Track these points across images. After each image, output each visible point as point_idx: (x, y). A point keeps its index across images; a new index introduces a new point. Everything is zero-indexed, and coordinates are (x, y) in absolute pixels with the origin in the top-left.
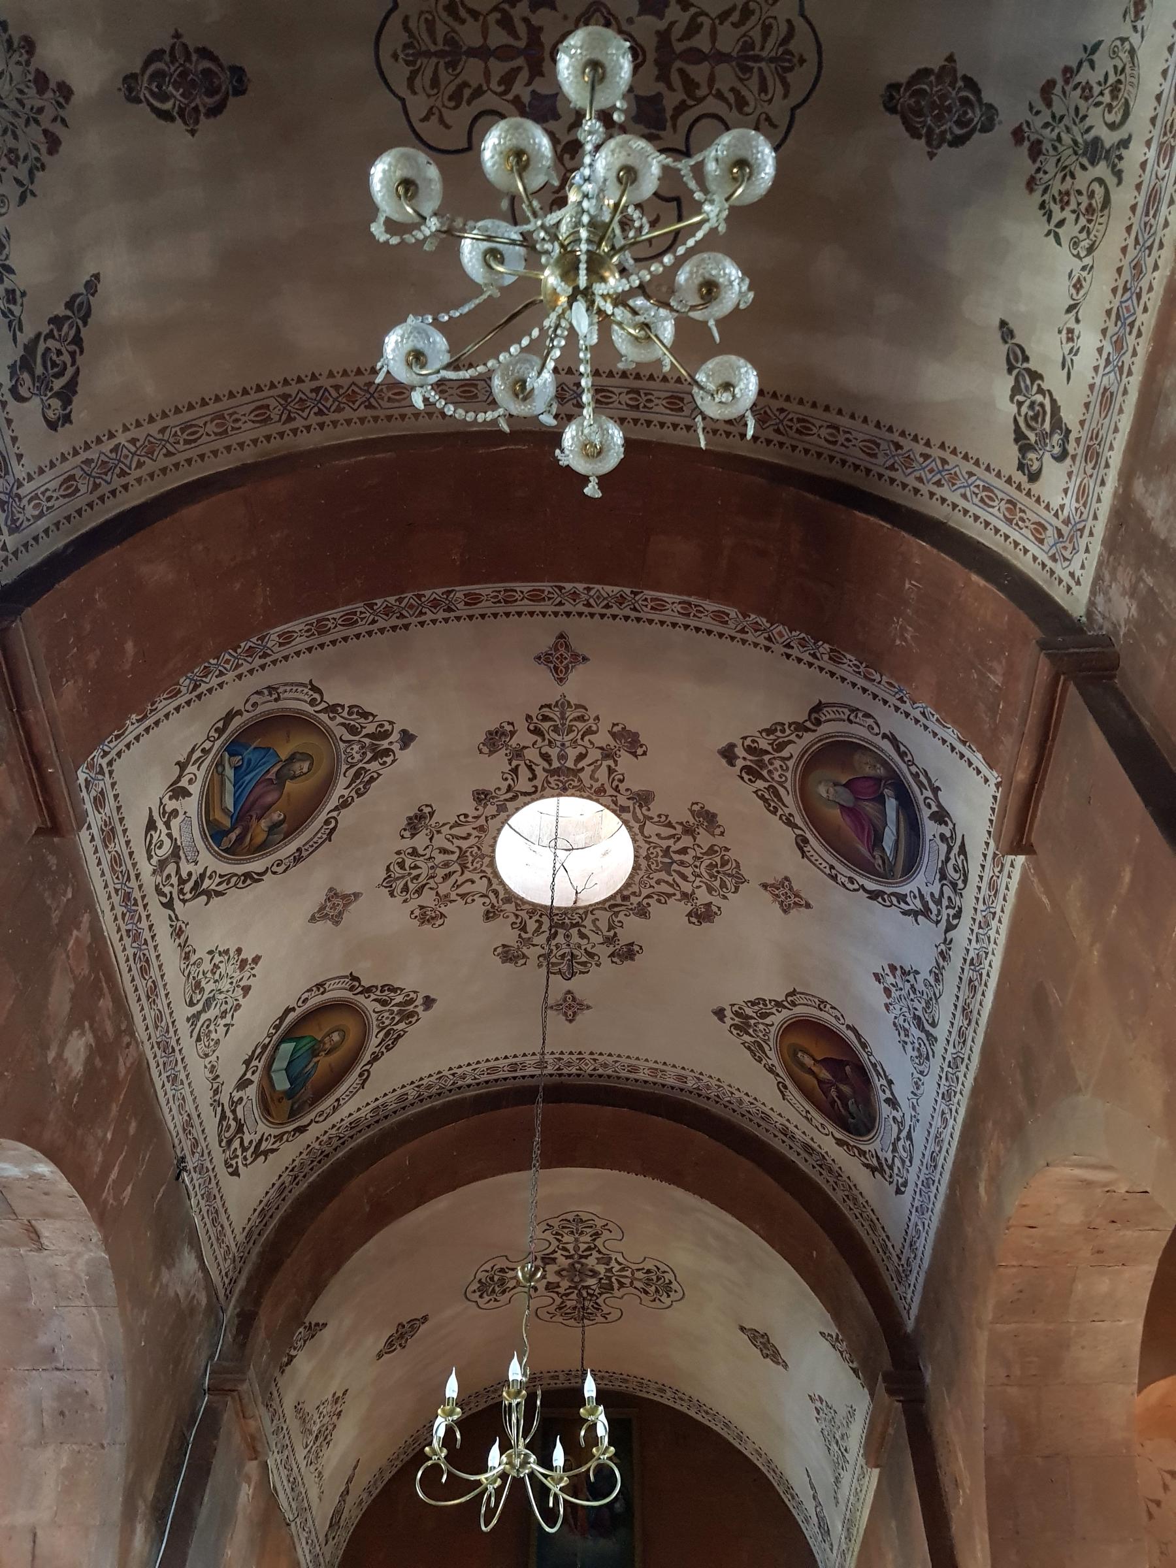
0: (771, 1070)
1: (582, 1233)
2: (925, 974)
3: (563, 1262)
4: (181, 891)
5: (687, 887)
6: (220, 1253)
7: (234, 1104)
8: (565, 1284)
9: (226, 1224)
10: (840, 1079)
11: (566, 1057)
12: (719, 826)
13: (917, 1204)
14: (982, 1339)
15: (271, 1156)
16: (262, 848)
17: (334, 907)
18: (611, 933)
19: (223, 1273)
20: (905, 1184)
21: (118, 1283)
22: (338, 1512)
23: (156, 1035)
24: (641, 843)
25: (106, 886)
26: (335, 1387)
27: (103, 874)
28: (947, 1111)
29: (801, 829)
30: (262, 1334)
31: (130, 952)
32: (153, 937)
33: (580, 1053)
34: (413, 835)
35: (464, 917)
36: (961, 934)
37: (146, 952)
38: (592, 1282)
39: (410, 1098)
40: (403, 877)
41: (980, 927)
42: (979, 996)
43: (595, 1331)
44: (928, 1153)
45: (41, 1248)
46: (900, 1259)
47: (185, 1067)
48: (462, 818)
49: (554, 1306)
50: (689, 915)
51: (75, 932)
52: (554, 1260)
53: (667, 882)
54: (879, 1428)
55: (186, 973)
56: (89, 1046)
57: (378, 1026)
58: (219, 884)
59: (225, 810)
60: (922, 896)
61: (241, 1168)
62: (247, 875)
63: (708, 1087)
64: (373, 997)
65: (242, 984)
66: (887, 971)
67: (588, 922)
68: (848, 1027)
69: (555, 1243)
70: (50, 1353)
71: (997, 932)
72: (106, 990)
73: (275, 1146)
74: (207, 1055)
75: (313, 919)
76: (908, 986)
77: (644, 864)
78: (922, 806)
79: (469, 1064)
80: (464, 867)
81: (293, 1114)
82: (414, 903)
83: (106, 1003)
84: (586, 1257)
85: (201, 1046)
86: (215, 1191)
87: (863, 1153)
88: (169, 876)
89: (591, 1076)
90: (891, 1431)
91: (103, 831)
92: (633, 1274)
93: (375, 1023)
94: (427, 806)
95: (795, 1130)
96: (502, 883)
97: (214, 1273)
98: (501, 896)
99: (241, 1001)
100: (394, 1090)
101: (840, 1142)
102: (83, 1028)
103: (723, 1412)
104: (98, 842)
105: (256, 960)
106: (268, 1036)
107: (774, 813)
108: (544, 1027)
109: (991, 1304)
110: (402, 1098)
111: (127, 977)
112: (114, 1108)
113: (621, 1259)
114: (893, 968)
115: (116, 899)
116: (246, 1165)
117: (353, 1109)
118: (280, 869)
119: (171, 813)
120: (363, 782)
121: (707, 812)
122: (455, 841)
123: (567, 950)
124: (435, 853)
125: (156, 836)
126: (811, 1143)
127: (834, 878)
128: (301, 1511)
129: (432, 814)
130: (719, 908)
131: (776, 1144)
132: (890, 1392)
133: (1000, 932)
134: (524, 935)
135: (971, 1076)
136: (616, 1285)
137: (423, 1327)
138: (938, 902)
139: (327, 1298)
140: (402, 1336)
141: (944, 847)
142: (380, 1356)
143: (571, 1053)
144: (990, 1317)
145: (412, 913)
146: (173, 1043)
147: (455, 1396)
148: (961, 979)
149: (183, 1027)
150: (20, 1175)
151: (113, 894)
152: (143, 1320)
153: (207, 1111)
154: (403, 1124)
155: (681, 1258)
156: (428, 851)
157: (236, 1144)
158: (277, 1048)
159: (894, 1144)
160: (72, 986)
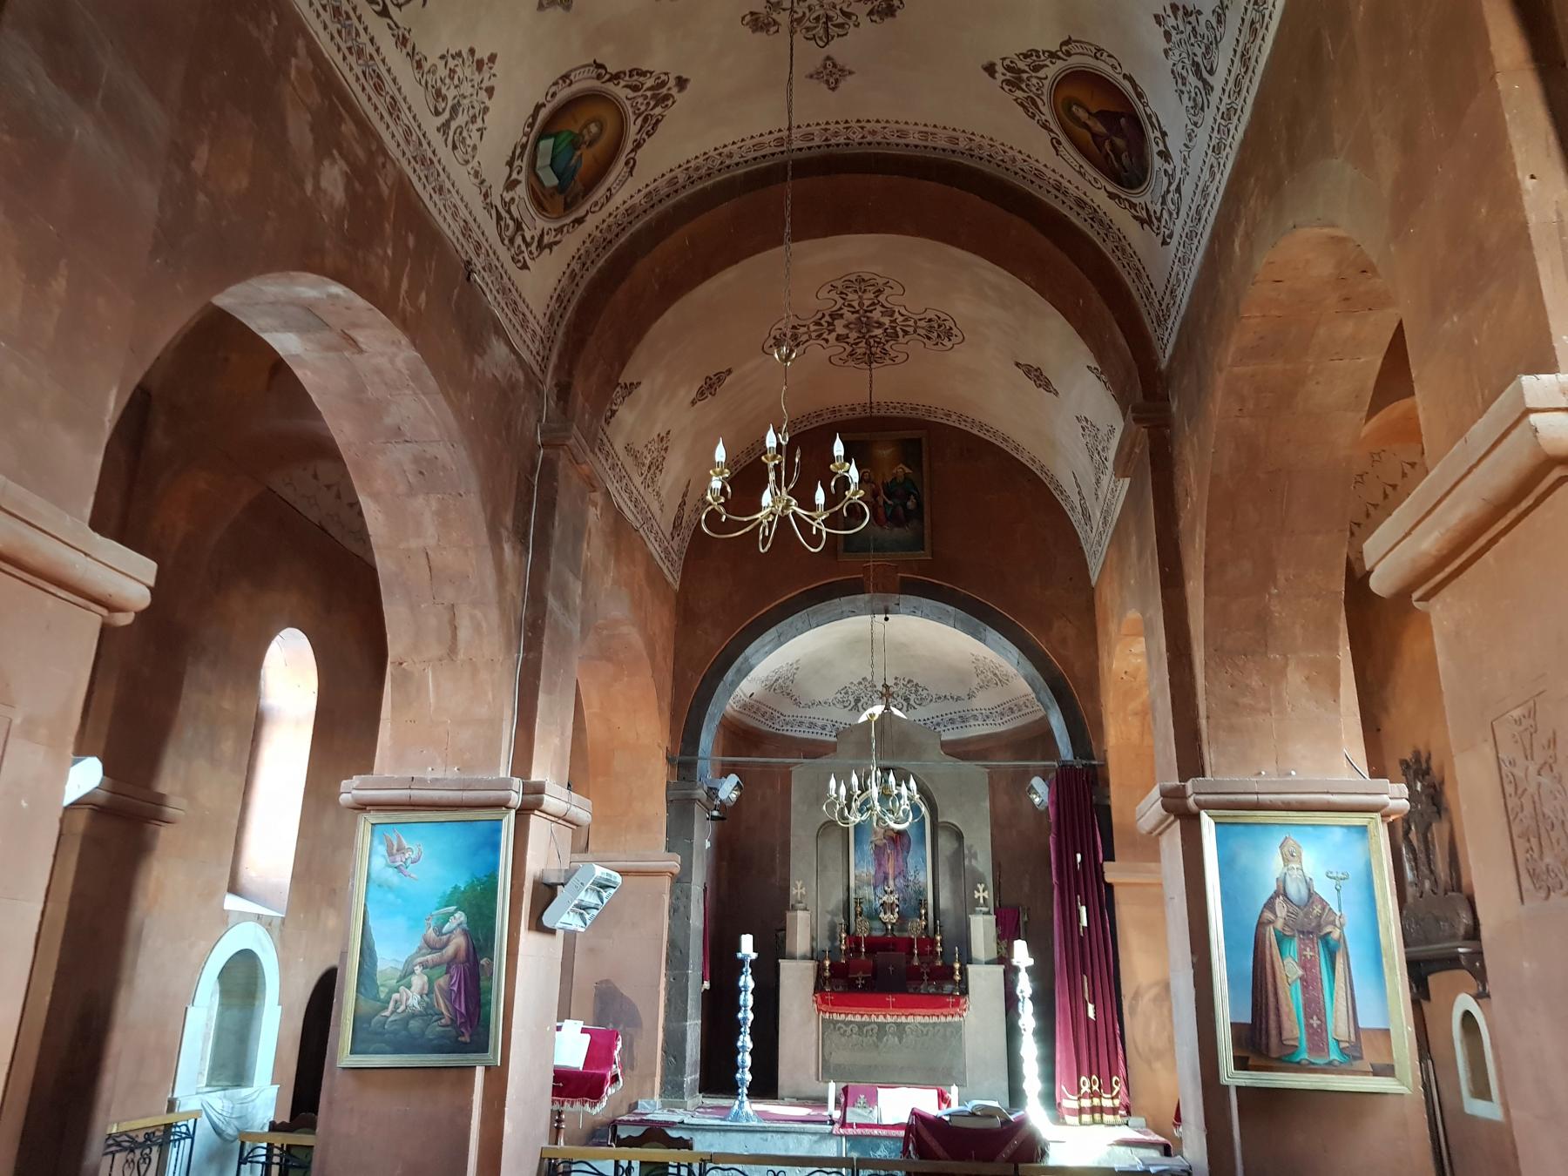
0: (1045, 126)
2: (1207, 15)
8: (853, 335)
10: (1112, 129)
11: (832, 127)
14: (1221, 379)
15: (555, 248)
20: (1171, 236)
26: (659, 429)
30: (580, 399)
32: (378, 50)
38: (878, 332)
42: (1259, 41)
43: (879, 372)
44: (1194, 207)
45: (361, 351)
51: (293, 61)
54: (1127, 449)
63: (980, 147)
64: (622, 83)
65: (484, 85)
66: (1169, 11)
68: (1125, 76)
70: (398, 431)
74: (467, 162)
76: (1189, 28)
81: (568, 207)
83: (348, 128)
85: (459, 153)
87: (1133, 206)
97: (525, 355)
101: (1111, 196)
102: (332, 155)
105: (492, 58)
109: (1232, 349)
110: (673, 181)
111: (363, 98)
114: (1174, 8)
115: (326, 16)
123: (821, 12)
128: (646, 520)
135: (1241, 129)
136: (901, 334)
142: (693, 403)
149: (436, 139)
151: (321, 11)
154: (678, 207)
155: (961, 308)
157: (519, 240)
160: (309, 117)
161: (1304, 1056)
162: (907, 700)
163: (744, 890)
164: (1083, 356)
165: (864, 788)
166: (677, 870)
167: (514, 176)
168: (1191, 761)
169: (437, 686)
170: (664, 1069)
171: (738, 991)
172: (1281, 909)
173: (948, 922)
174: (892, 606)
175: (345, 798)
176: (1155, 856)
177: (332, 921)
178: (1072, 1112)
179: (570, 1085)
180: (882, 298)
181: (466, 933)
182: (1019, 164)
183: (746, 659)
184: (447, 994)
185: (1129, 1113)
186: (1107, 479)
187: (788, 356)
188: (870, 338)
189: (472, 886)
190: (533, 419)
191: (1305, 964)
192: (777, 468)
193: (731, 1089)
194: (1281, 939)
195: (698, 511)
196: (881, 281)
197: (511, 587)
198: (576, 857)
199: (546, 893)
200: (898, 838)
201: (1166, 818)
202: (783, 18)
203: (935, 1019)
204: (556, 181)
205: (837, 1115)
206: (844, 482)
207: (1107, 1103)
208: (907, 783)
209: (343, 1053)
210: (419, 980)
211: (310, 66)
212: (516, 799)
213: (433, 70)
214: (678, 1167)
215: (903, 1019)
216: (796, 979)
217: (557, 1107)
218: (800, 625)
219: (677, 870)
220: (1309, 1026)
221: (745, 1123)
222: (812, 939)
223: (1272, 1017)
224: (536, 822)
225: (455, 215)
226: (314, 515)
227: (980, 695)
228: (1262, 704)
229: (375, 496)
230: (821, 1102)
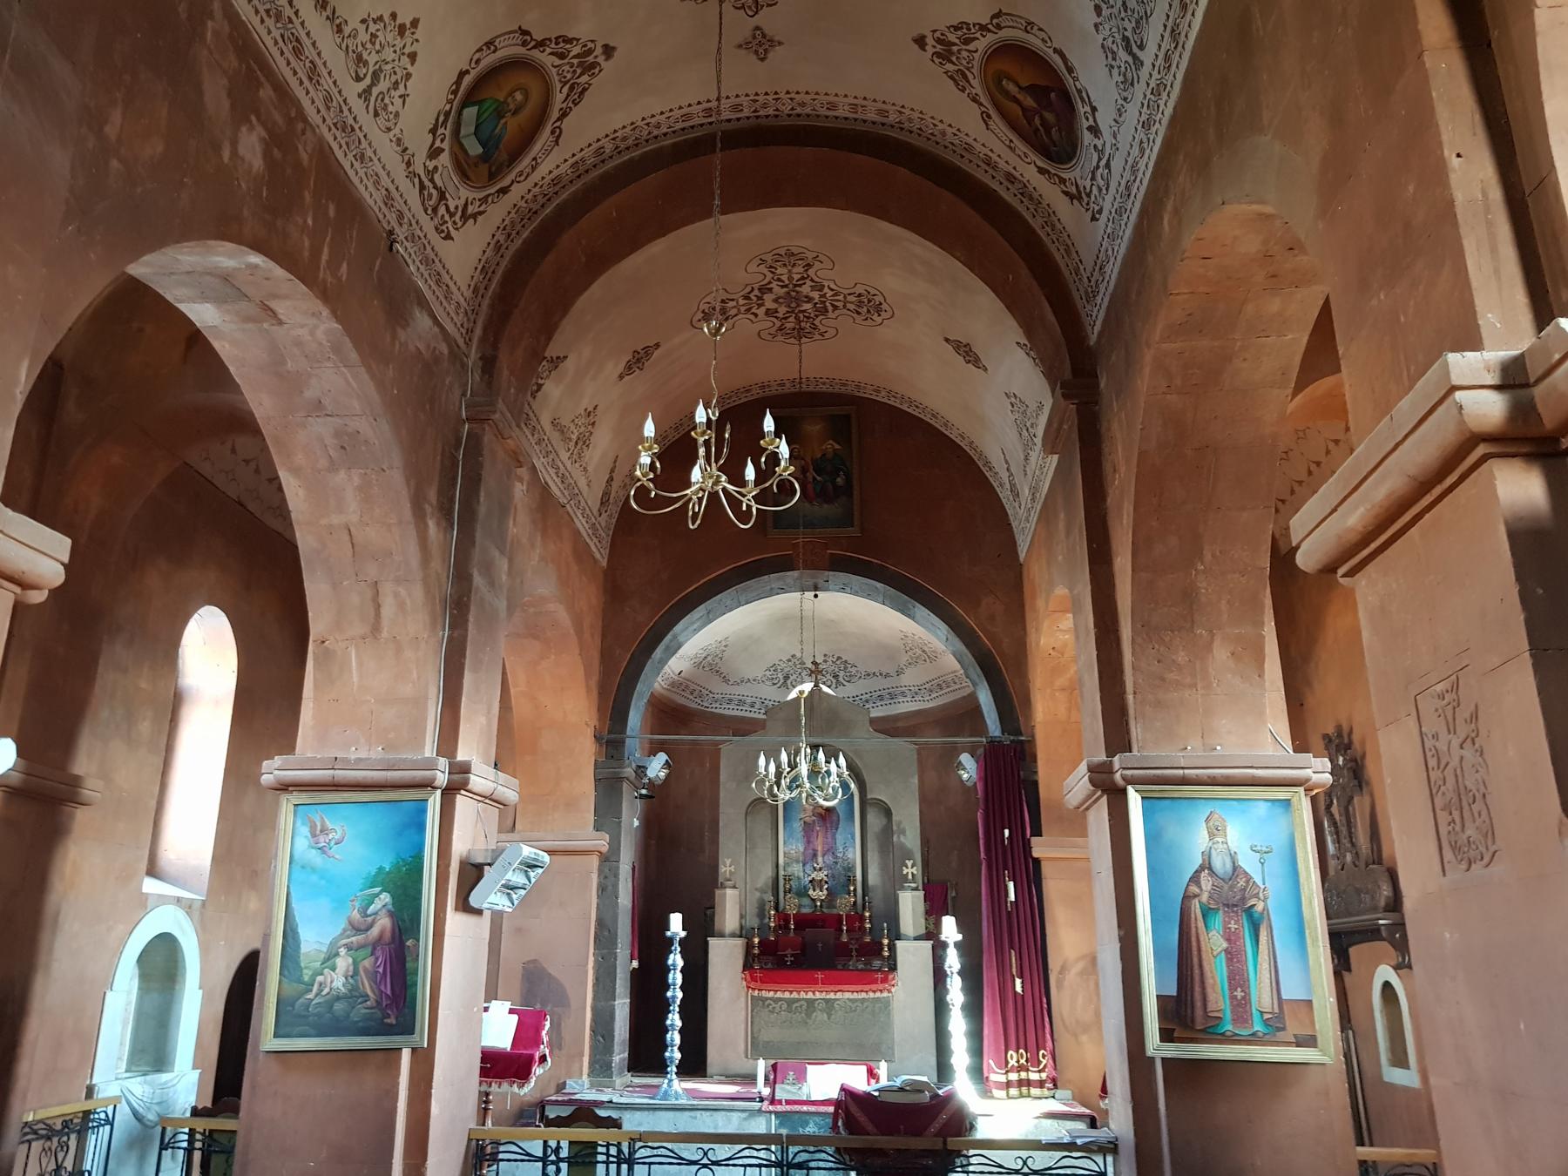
0: (974, 100)
7: (431, 173)
8: (782, 310)
9: (451, 284)
10: (1044, 106)
11: (761, 98)
13: (1109, 230)
14: (1148, 356)
15: (480, 218)
20: (1100, 212)
22: (606, 494)
26: (586, 403)
30: (506, 373)
31: (276, 34)
32: (296, 13)
38: (807, 306)
44: (1123, 183)
45: (281, 323)
51: (210, 24)
56: (262, 140)
64: (548, 50)
65: (407, 51)
68: (1055, 51)
72: (262, 79)
74: (389, 129)
81: (493, 177)
83: (266, 93)
85: (381, 120)
87: (1062, 181)
97: (449, 327)
101: (1041, 171)
105: (415, 23)
108: (719, 82)
109: (1160, 327)
110: (599, 152)
111: (281, 62)
112: (307, 196)
131: (979, 175)
135: (1171, 105)
136: (830, 308)
139: (567, 329)
142: (621, 377)
149: (357, 105)
154: (604, 178)
155: (891, 283)
157: (442, 210)
158: (460, 113)
160: (225, 81)
161: (1228, 1027)
162: (836, 676)
163: (672, 869)
164: (1013, 332)
165: (793, 765)
166: (605, 849)
167: (438, 144)
168: (1117, 737)
169: (360, 664)
171: (666, 970)
172: (1206, 882)
173: (877, 899)
174: (821, 582)
175: (266, 779)
178: (999, 1086)
179: (497, 1066)
180: (811, 272)
181: (391, 914)
182: (949, 137)
183: (675, 637)
184: (373, 976)
185: (1056, 1086)
186: (1036, 454)
189: (397, 867)
190: (457, 392)
191: (1230, 937)
192: (707, 443)
195: (626, 487)
196: (810, 255)
197: (436, 565)
198: (504, 837)
199: (473, 873)
200: (827, 816)
203: (863, 995)
205: (766, 1092)
206: (774, 458)
207: (1034, 1076)
208: (836, 760)
209: (266, 1036)
210: (343, 963)
211: (227, 29)
212: (442, 779)
214: (608, 1146)
215: (832, 996)
216: (725, 957)
217: (484, 1088)
219: (605, 849)
220: (1233, 998)
221: (674, 1101)
222: (742, 916)
223: (1197, 989)
224: (462, 802)
225: (377, 183)
226: (232, 491)
227: (908, 671)
228: (1188, 680)
229: (296, 471)
230: (751, 1079)
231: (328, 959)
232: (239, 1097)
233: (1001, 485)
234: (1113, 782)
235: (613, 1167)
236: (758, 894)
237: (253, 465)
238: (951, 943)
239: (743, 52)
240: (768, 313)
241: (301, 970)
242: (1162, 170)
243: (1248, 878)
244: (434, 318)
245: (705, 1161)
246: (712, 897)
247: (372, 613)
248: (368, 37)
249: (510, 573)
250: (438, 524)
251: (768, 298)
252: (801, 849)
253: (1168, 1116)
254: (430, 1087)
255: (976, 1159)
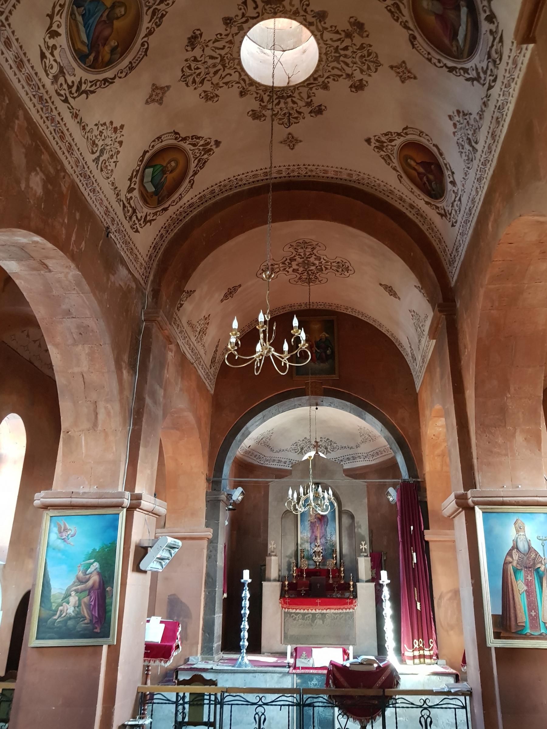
0: (395, 169)
1: (307, 248)
2: (475, 115)
3: (299, 260)
4: (71, 92)
5: (349, 71)
6: (138, 266)
7: (129, 200)
8: (301, 269)
9: (138, 254)
10: (428, 171)
11: (291, 168)
12: (366, 31)
14: (482, 292)
15: (153, 223)
16: (109, 63)
17: (157, 95)
18: (309, 100)
19: (141, 274)
20: (456, 222)
21: (89, 284)
22: (214, 358)
23: (78, 170)
24: (322, 45)
25: (27, 94)
26: (204, 313)
27: (23, 87)
28: (479, 187)
29: (412, 30)
31: (52, 128)
32: (62, 119)
33: (298, 165)
34: (193, 49)
35: (229, 95)
36: (496, 91)
37: (60, 128)
38: (313, 268)
39: (216, 191)
40: (191, 75)
41: (506, 87)
42: (500, 127)
43: (314, 287)
44: (468, 208)
45: (50, 271)
46: (451, 256)
47: (98, 185)
48: (219, 36)
49: (297, 278)
50: (351, 87)
51: (17, 122)
52: (295, 260)
53: (338, 68)
54: (435, 325)
55: (86, 137)
57: (194, 157)
58: (91, 86)
59: (83, 42)
60: (477, 69)
61: (139, 229)
62: (105, 80)
63: (363, 179)
64: (188, 142)
65: (118, 140)
66: (456, 113)
67: (296, 94)
68: (434, 145)
69: (295, 253)
71: (514, 90)
72: (44, 150)
73: (154, 218)
74: (108, 178)
75: (147, 102)
76: (465, 121)
77: (324, 57)
78: (482, 12)
79: (243, 174)
80: (224, 66)
81: (160, 203)
82: (200, 90)
83: (45, 157)
84: (310, 258)
85: (104, 173)
86: (129, 240)
87: (437, 208)
88: (61, 85)
89: (305, 176)
90: (440, 326)
91: (16, 62)
92: (331, 263)
93: (192, 156)
94: (198, 30)
95: (405, 197)
96: (247, 75)
97: (137, 275)
98: (247, 82)
99: (119, 149)
100: (208, 188)
101: (427, 203)
102: (36, 170)
103: (372, 317)
104: (15, 68)
105: (122, 127)
106: (138, 166)
107: (397, 20)
109: (487, 277)
110: (213, 192)
111: (54, 143)
112: (65, 209)
113: (325, 258)
114: (458, 112)
115: (35, 100)
116: (141, 227)
117: (189, 199)
118: (123, 75)
119: (52, 47)
120: (158, 17)
121: (359, 22)
122: (217, 50)
123: (286, 111)
124: (207, 59)
125: (47, 62)
126: (413, 204)
127: (430, 60)
129: (201, 35)
130: (367, 82)
132: (440, 311)
133: (515, 89)
134: (263, 104)
136: (324, 269)
137: (239, 289)
138: (485, 73)
139: (196, 275)
140: (231, 293)
141: (491, 38)
142: (222, 301)
143: (294, 165)
144: (486, 282)
145: (200, 95)
146: (89, 173)
147: (237, 328)
148: (492, 117)
150: (28, 242)
152: (106, 296)
153: (115, 205)
155: (353, 256)
156: (203, 58)
159: (453, 204)
160: (24, 150)
161: (528, 631)
162: (326, 448)
163: (244, 547)
164: (412, 280)
167: (132, 186)
168: (469, 481)
169: (87, 443)
170: (203, 640)
171: (240, 631)
172: (516, 556)
173: (347, 560)
174: (319, 402)
175: (37, 503)
176: (451, 526)
177: (31, 566)
178: (409, 658)
179: (154, 651)
180: (315, 251)
181: (99, 574)
182: (382, 187)
183: (247, 429)
184: (88, 606)
185: (438, 658)
186: (425, 340)
187: (270, 276)
188: (309, 274)
189: (103, 549)
190: (140, 307)
191: (528, 584)
192: (264, 332)
193: (237, 649)
194: (516, 571)
195: (223, 354)
197: (127, 393)
198: (159, 530)
199: (142, 551)
200: (322, 519)
201: (458, 509)
202: (268, 113)
203: (340, 611)
204: (154, 189)
205: (292, 661)
206: (298, 340)
207: (427, 653)
208: (328, 491)
209: (32, 639)
210: (73, 599)
211: (26, 125)
212: (127, 503)
213: (91, 131)
214: (210, 695)
215: (325, 611)
216: (271, 591)
217: (146, 663)
218: (274, 411)
220: (530, 615)
221: (244, 668)
222: (279, 570)
223: (512, 611)
224: (137, 515)
225: (101, 204)
226: (26, 355)
227: (362, 446)
228: (504, 452)
229: (56, 345)
230: (283, 654)
231: (65, 598)
232: (17, 669)
233: (407, 355)
234: (468, 504)
235: (212, 707)
236: (287, 559)
237: (38, 343)
238: (385, 584)
239: (283, 145)
240: (294, 270)
241: (51, 603)
242: (488, 201)
243: (537, 554)
244: (128, 269)
245: (260, 703)
246: (265, 560)
247: (93, 417)
248: (98, 133)
249: (164, 397)
250: (128, 372)
251: (294, 263)
252: (309, 536)
253: (498, 677)
254: (117, 666)
255: (400, 700)
